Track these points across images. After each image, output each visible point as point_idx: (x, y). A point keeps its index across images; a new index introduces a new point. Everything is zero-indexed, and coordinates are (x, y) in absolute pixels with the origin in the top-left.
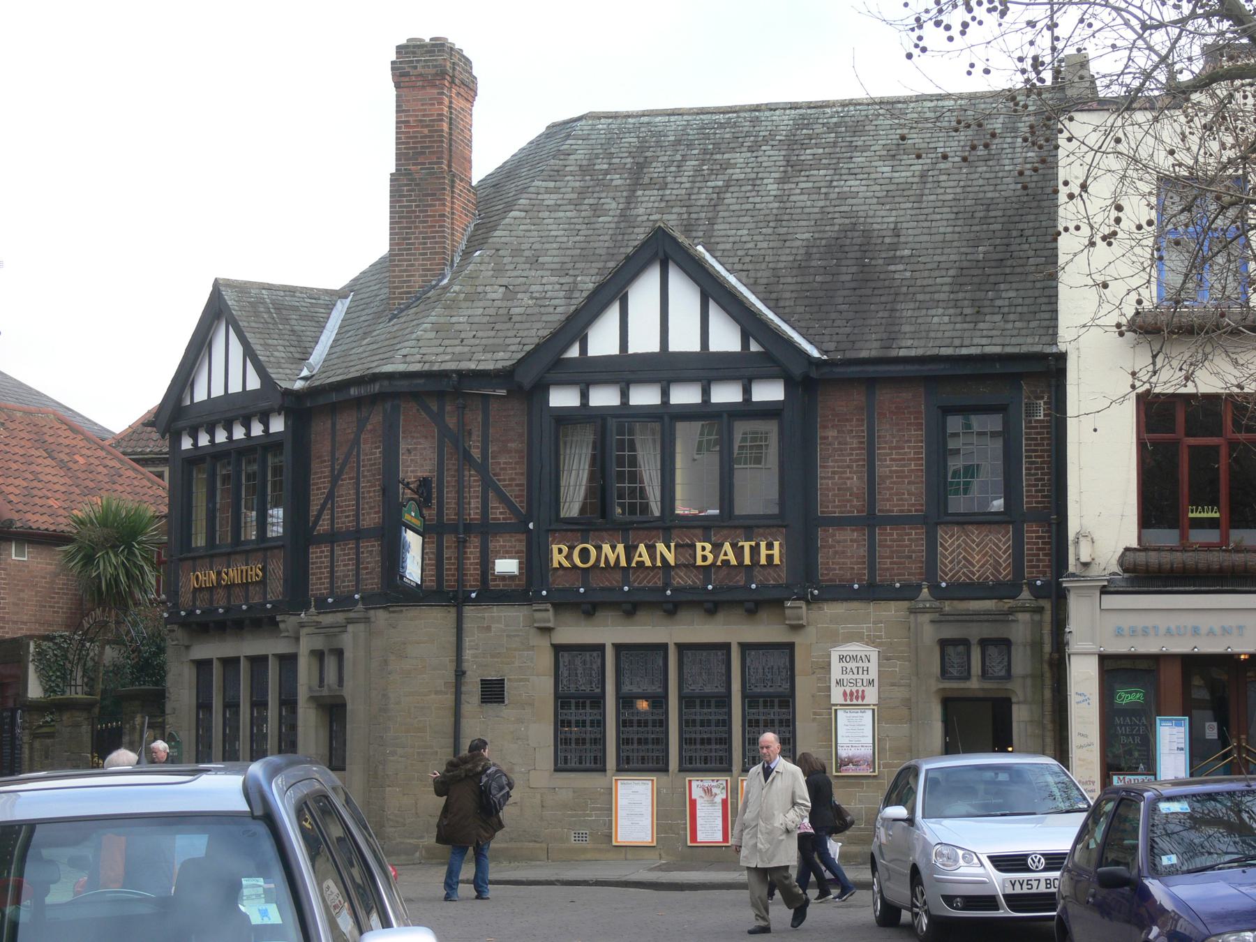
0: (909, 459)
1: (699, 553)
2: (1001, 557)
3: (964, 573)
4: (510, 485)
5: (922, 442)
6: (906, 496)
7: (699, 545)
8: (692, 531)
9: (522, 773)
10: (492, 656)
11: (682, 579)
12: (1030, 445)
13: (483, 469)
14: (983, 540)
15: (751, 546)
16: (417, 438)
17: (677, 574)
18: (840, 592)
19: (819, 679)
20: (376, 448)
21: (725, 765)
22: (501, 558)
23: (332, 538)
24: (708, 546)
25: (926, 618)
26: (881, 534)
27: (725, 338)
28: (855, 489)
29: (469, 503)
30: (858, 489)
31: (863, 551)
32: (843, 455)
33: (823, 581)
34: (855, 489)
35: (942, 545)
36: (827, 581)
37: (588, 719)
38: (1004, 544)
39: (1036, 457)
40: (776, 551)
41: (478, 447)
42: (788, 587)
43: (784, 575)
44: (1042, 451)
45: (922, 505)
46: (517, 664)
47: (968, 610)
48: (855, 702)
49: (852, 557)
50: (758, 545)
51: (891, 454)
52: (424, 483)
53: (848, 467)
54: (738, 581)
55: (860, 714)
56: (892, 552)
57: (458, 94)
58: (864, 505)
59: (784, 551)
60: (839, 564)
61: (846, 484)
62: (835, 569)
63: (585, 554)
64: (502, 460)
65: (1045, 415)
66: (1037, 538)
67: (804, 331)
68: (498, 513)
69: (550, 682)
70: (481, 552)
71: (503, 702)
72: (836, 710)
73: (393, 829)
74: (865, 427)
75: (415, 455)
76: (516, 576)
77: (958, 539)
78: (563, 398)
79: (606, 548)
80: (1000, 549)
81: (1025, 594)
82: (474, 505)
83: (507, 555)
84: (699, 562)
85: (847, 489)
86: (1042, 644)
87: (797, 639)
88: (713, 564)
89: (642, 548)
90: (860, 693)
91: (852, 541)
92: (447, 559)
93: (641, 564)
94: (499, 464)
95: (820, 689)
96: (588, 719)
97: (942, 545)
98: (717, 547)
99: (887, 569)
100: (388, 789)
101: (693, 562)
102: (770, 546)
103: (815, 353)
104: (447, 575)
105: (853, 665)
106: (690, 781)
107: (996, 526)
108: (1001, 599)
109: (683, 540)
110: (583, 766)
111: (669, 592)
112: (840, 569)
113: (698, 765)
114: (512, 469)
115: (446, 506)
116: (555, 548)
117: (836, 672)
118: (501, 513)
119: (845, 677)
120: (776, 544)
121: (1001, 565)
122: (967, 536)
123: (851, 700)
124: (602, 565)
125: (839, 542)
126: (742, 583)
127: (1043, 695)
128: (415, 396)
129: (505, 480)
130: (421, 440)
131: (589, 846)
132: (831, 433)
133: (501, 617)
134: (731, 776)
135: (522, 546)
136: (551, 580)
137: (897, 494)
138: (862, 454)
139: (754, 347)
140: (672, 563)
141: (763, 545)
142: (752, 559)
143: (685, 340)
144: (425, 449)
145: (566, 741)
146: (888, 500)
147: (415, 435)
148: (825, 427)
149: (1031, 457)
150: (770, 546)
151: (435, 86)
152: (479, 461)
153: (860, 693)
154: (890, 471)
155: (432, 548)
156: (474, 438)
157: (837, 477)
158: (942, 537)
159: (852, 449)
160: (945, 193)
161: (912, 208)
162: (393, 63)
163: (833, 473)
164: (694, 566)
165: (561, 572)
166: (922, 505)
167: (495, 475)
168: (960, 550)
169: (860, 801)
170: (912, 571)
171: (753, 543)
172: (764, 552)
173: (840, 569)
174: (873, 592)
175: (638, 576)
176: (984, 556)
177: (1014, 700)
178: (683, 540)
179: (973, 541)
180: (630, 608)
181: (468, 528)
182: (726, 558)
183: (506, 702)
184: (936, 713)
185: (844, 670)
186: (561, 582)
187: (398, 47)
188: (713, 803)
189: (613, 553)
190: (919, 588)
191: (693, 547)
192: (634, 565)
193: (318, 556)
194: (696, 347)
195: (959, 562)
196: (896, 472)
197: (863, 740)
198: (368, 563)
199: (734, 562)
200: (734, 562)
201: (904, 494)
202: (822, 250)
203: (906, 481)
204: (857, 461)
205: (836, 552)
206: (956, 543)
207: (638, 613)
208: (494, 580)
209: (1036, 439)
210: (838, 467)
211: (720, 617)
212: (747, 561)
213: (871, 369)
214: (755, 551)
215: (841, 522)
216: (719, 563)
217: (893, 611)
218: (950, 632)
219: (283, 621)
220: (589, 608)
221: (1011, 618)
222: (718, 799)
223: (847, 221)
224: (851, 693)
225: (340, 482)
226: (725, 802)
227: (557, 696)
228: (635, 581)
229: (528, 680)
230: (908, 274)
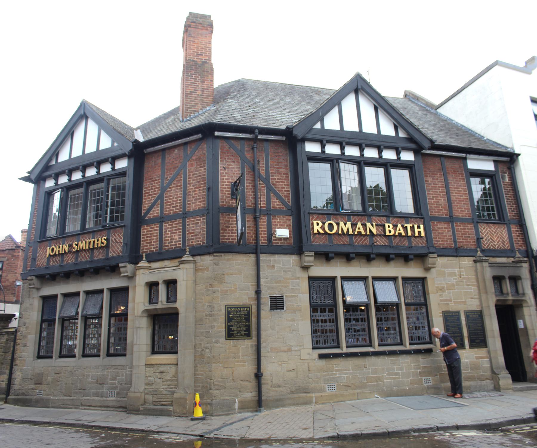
1: (387, 229)
3: (491, 245)
4: (282, 191)
7: (387, 225)
8: (381, 217)
9: (296, 351)
10: (276, 282)
11: (380, 242)
13: (266, 181)
14: (496, 231)
15: (410, 227)
16: (229, 162)
19: (440, 295)
20: (201, 167)
22: (278, 228)
23: (161, 220)
24: (391, 226)
26: (456, 226)
28: (443, 205)
30: (444, 205)
31: (451, 233)
34: (443, 205)
37: (327, 318)
39: (509, 197)
40: (422, 229)
41: (263, 170)
44: (510, 194)
46: (290, 287)
50: (413, 226)
54: (405, 244)
61: (439, 202)
62: (439, 241)
63: (331, 226)
65: (509, 180)
66: (516, 231)
68: (276, 204)
69: (307, 297)
71: (283, 309)
73: (218, 391)
74: (443, 178)
75: (228, 171)
76: (288, 238)
77: (487, 229)
78: (312, 148)
79: (342, 224)
83: (281, 226)
84: (388, 233)
87: (428, 275)
89: (359, 225)
91: (445, 228)
92: (248, 227)
93: (360, 233)
94: (275, 179)
96: (327, 318)
97: (481, 232)
98: (395, 226)
100: (214, 365)
101: (383, 233)
102: (419, 227)
104: (248, 236)
107: (500, 225)
108: (508, 257)
110: (359, 344)
113: (321, 345)
114: (282, 182)
115: (246, 199)
116: (315, 223)
118: (277, 205)
120: (422, 226)
122: (490, 229)
125: (439, 228)
126: (407, 244)
129: (278, 188)
130: (232, 163)
133: (280, 260)
135: (290, 222)
136: (312, 240)
137: (460, 208)
138: (443, 190)
139: (402, 134)
141: (416, 226)
143: (370, 128)
144: (233, 168)
146: (456, 211)
147: (228, 160)
148: (427, 176)
150: (419, 227)
152: (265, 177)
154: (456, 198)
157: (435, 198)
159: (439, 187)
163: (433, 197)
164: (385, 236)
165: (317, 236)
166: (470, 214)
167: (273, 184)
168: (488, 235)
170: (471, 244)
172: (416, 230)
173: (442, 241)
175: (357, 240)
176: (498, 237)
182: (399, 232)
183: (285, 309)
186: (318, 241)
189: (346, 227)
191: (384, 226)
192: (356, 233)
193: (145, 230)
194: (357, 130)
195: (489, 240)
196: (458, 198)
198: (194, 230)
199: (403, 234)
200: (403, 234)
204: (442, 192)
205: (439, 233)
206: (487, 232)
208: (276, 240)
210: (435, 194)
214: (412, 228)
217: (467, 262)
219: (125, 267)
225: (168, 189)
227: (311, 306)
228: (356, 242)
229: (297, 296)
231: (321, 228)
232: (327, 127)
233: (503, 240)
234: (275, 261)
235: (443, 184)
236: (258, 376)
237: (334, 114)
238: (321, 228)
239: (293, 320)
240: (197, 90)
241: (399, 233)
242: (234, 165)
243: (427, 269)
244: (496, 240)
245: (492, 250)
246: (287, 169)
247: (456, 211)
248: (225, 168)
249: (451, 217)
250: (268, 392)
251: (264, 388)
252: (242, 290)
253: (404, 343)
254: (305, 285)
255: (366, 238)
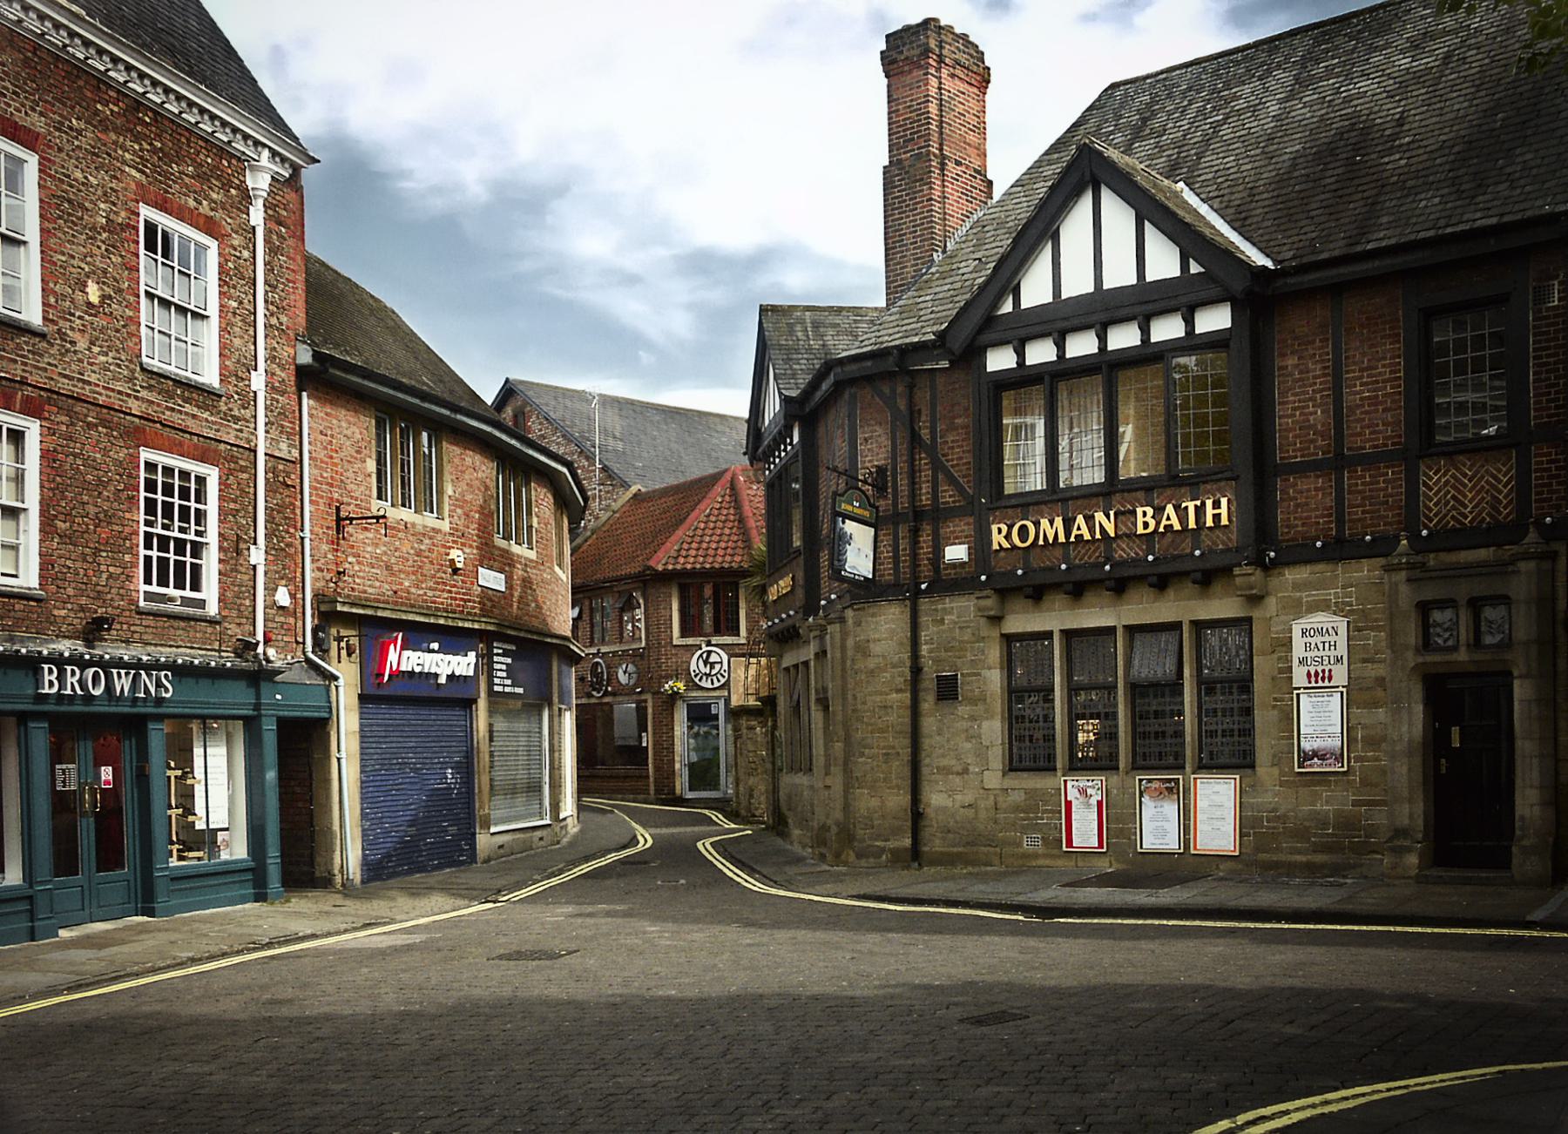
0: (1384, 381)
2: (1500, 492)
5: (1399, 357)
6: (1381, 428)
7: (1139, 511)
11: (1123, 551)
12: (1540, 342)
13: (932, 451)
15: (1196, 506)
17: (1118, 546)
18: (1299, 554)
21: (1140, 762)
24: (1150, 511)
25: (1403, 575)
27: (1164, 262)
29: (921, 489)
31: (1330, 501)
32: (1305, 386)
33: (1284, 541)
35: (1425, 484)
36: (1288, 541)
38: (1504, 476)
39: (1548, 356)
40: (1224, 511)
42: (1238, 550)
43: (1234, 537)
45: (1400, 436)
47: (1459, 563)
48: (1320, 684)
49: (1317, 509)
50: (1203, 504)
51: (1362, 377)
52: (881, 470)
53: (1310, 399)
55: (1326, 698)
56: (1363, 498)
57: (953, 76)
58: (1329, 445)
59: (1233, 509)
60: (1301, 518)
62: (1297, 526)
63: (1023, 532)
64: (950, 438)
65: (1560, 300)
67: (1263, 245)
68: (948, 496)
70: (933, 540)
72: (1298, 695)
74: (1330, 349)
77: (1444, 475)
78: (1000, 360)
79: (1045, 523)
80: (1499, 481)
81: (1532, 536)
82: (925, 488)
84: (1140, 530)
85: (1310, 427)
86: (1554, 599)
87: (1256, 614)
88: (1156, 531)
89: (1080, 520)
90: (1327, 674)
91: (1316, 489)
95: (1281, 671)
97: (1425, 484)
98: (1159, 511)
99: (1359, 520)
102: (1217, 505)
103: (1259, 259)
105: (1318, 639)
106: (1065, 781)
108: (1499, 546)
109: (1124, 506)
111: (1107, 567)
112: (1303, 525)
116: (994, 528)
117: (1298, 650)
119: (1308, 654)
120: (1224, 501)
121: (1500, 502)
123: (1317, 682)
124: (1041, 542)
127: (1555, 665)
128: (868, 379)
130: (877, 428)
131: (1040, 852)
132: (1291, 361)
134: (1184, 774)
139: (1195, 268)
140: (1112, 535)
141: (1209, 503)
142: (1197, 522)
143: (1120, 274)
145: (1021, 739)
146: (1360, 434)
148: (1283, 355)
149: (1540, 357)
150: (1217, 505)
151: (920, 67)
153: (1327, 674)
154: (1361, 399)
155: (886, 541)
156: (923, 418)
158: (1426, 474)
159: (1315, 377)
160: (1470, 68)
161: (1426, 93)
162: (882, 53)
163: (1294, 409)
165: (1002, 554)
167: (944, 455)
169: (1327, 802)
171: (1198, 503)
172: (1210, 511)
173: (1303, 525)
174: (1340, 549)
176: (1478, 492)
177: (1516, 673)
178: (1124, 506)
179: (1465, 475)
180: (1077, 589)
181: (918, 515)
184: (1417, 692)
185: (1307, 647)
187: (887, 36)
188: (1089, 805)
189: (1052, 528)
190: (1397, 540)
191: (1134, 513)
195: (1447, 503)
197: (1330, 730)
199: (1177, 527)
200: (1177, 527)
201: (1377, 425)
202: (1310, 158)
203: (1380, 408)
205: (1297, 506)
207: (1086, 594)
208: (945, 569)
209: (1548, 333)
210: (1299, 401)
211: (1171, 593)
212: (1192, 524)
213: (1333, 272)
214: (1200, 511)
215: (1302, 469)
216: (1161, 529)
217: (1365, 571)
218: (1430, 593)
220: (1037, 592)
221: (1510, 568)
222: (1094, 801)
223: (1347, 123)
224: (1317, 674)
226: (1100, 803)
230: (1403, 162)
231: (1006, 537)
232: (1026, 303)
233: (1494, 497)
234: (945, 609)
235: (1325, 368)
236: (917, 815)
237: (1040, 270)
238: (1006, 537)
239: (973, 718)
240: (905, 234)
241: (1165, 527)
242: (879, 430)
243: (1255, 600)
244: (1470, 501)
245: (1454, 530)
246: (967, 417)
247: (1360, 434)
248: (866, 440)
249: (1339, 455)
250: (935, 844)
251: (926, 834)
252: (894, 666)
253: (1013, 774)
254: (994, 653)
255: (1098, 548)
